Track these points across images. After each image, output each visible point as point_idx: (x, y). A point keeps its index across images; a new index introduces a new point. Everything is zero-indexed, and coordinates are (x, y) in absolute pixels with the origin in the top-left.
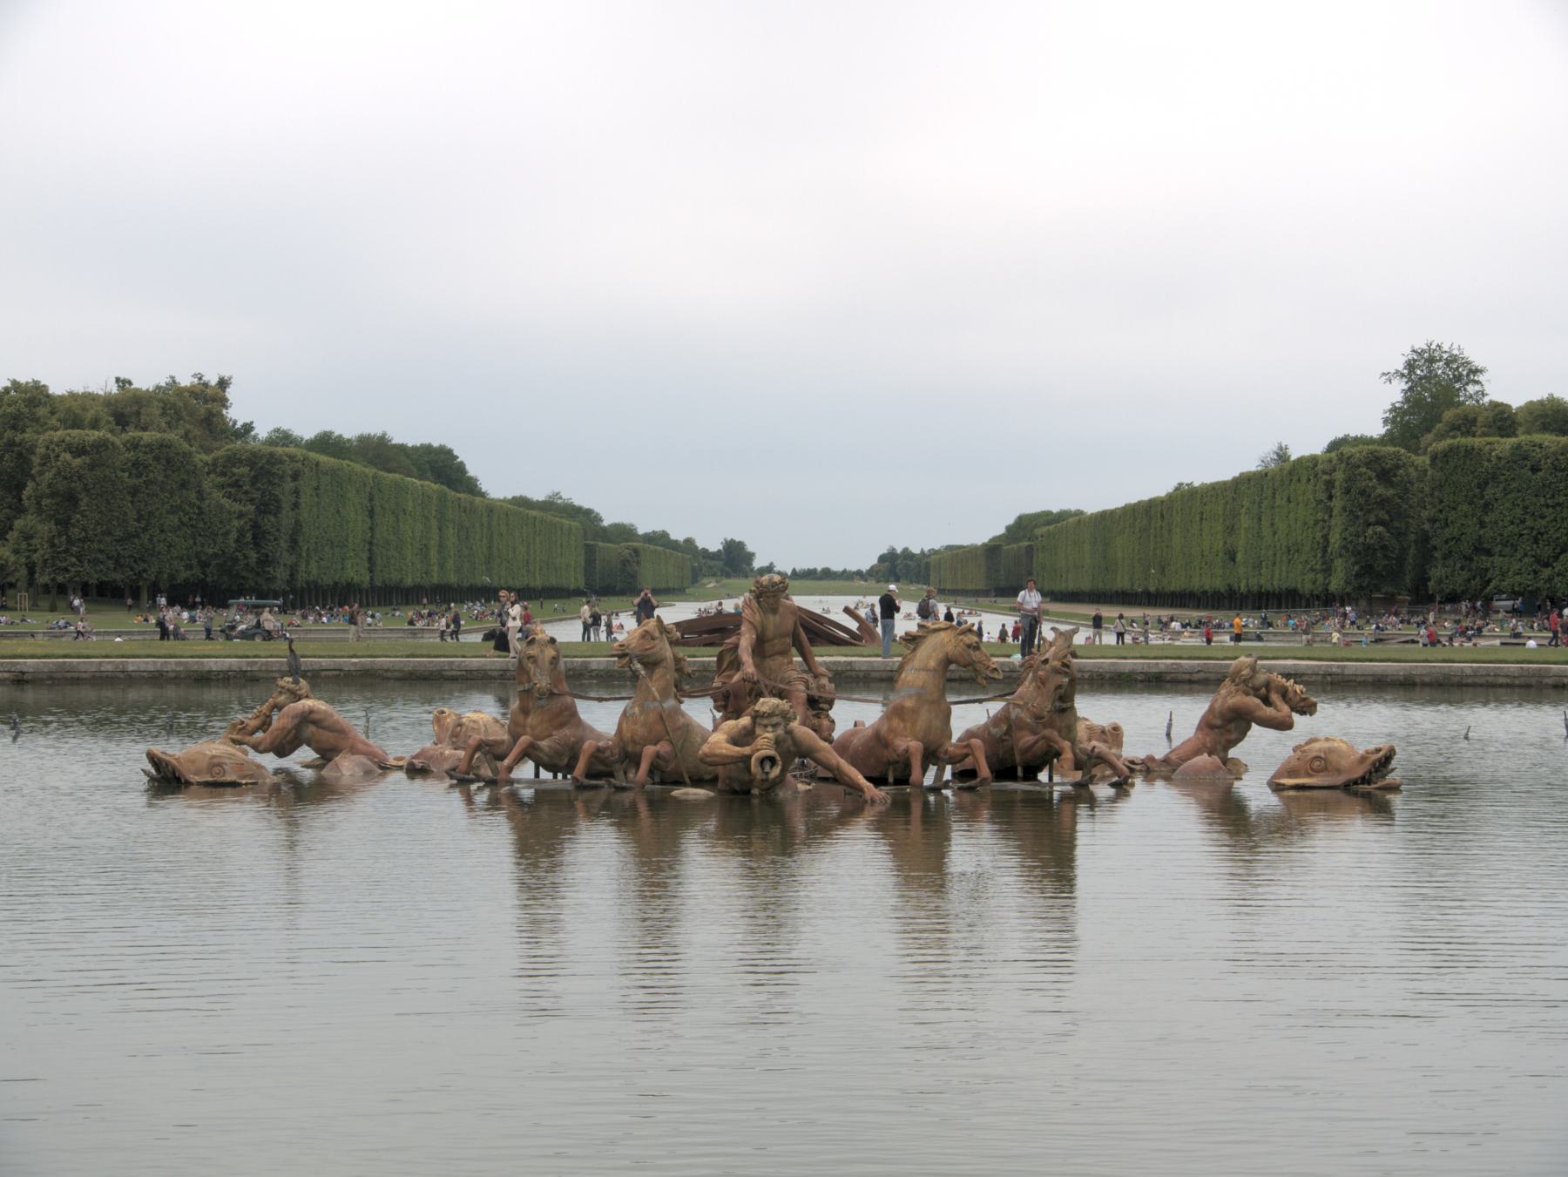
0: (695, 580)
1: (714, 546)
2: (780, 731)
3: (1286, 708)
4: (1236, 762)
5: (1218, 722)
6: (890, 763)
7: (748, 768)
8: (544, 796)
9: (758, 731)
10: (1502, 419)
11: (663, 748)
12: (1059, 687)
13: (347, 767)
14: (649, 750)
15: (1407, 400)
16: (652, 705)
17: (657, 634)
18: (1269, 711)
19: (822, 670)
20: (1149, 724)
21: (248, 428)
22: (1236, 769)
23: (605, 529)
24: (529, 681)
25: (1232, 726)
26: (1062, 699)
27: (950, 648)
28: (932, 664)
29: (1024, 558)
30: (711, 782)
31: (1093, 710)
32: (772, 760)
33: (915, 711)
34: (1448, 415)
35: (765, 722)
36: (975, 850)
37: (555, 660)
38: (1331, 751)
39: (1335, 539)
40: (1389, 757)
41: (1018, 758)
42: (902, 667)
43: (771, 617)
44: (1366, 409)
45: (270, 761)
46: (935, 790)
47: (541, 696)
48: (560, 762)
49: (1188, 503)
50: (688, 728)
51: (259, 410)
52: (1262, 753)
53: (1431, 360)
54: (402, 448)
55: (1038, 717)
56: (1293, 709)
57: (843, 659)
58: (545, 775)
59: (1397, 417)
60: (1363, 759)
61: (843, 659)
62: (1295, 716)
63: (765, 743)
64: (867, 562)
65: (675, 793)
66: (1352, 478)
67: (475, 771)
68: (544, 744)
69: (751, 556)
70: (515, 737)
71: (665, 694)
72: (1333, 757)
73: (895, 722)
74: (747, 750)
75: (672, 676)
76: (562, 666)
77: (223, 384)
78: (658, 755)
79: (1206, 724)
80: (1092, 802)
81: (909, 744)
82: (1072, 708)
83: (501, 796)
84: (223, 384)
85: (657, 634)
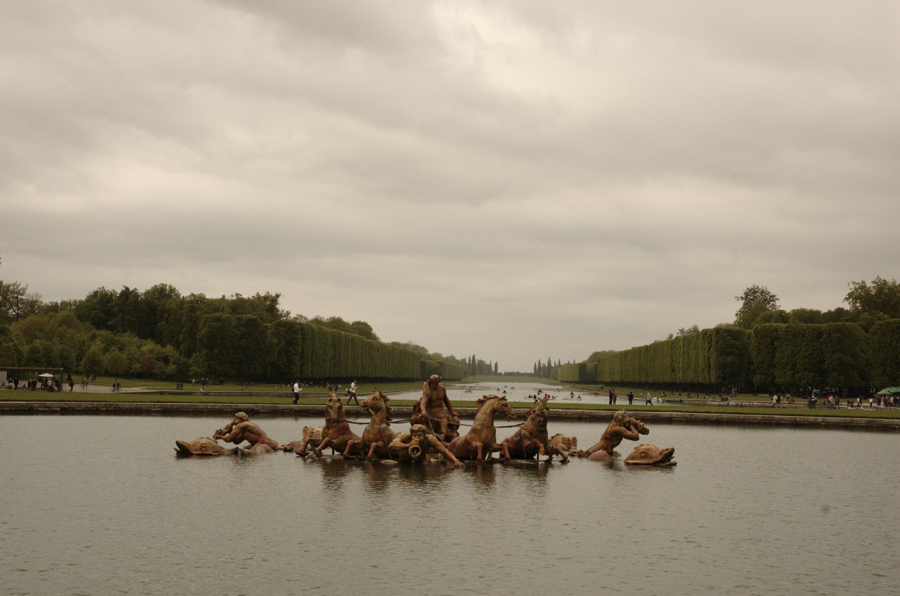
0: (465, 376)
2: (422, 438)
3: (636, 432)
4: (616, 453)
8: (334, 461)
10: (782, 316)
11: (380, 443)
12: (539, 422)
13: (259, 448)
14: (374, 444)
16: (376, 426)
19: (455, 413)
20: (590, 435)
21: (288, 313)
26: (541, 426)
27: (495, 406)
28: (488, 412)
31: (553, 429)
32: (417, 449)
33: (481, 431)
34: (762, 314)
37: (340, 408)
38: (649, 449)
39: (712, 361)
40: (672, 451)
42: (477, 412)
44: (725, 313)
45: (231, 446)
47: (334, 421)
48: (339, 448)
49: (655, 349)
52: (625, 448)
55: (531, 434)
56: (640, 432)
60: (661, 453)
62: (640, 435)
65: (383, 462)
67: (308, 450)
68: (335, 441)
70: (324, 438)
71: (382, 422)
72: (650, 452)
73: (473, 435)
74: (408, 445)
75: (384, 415)
76: (343, 410)
77: (278, 296)
78: (377, 446)
80: (552, 466)
81: (477, 444)
83: (319, 458)
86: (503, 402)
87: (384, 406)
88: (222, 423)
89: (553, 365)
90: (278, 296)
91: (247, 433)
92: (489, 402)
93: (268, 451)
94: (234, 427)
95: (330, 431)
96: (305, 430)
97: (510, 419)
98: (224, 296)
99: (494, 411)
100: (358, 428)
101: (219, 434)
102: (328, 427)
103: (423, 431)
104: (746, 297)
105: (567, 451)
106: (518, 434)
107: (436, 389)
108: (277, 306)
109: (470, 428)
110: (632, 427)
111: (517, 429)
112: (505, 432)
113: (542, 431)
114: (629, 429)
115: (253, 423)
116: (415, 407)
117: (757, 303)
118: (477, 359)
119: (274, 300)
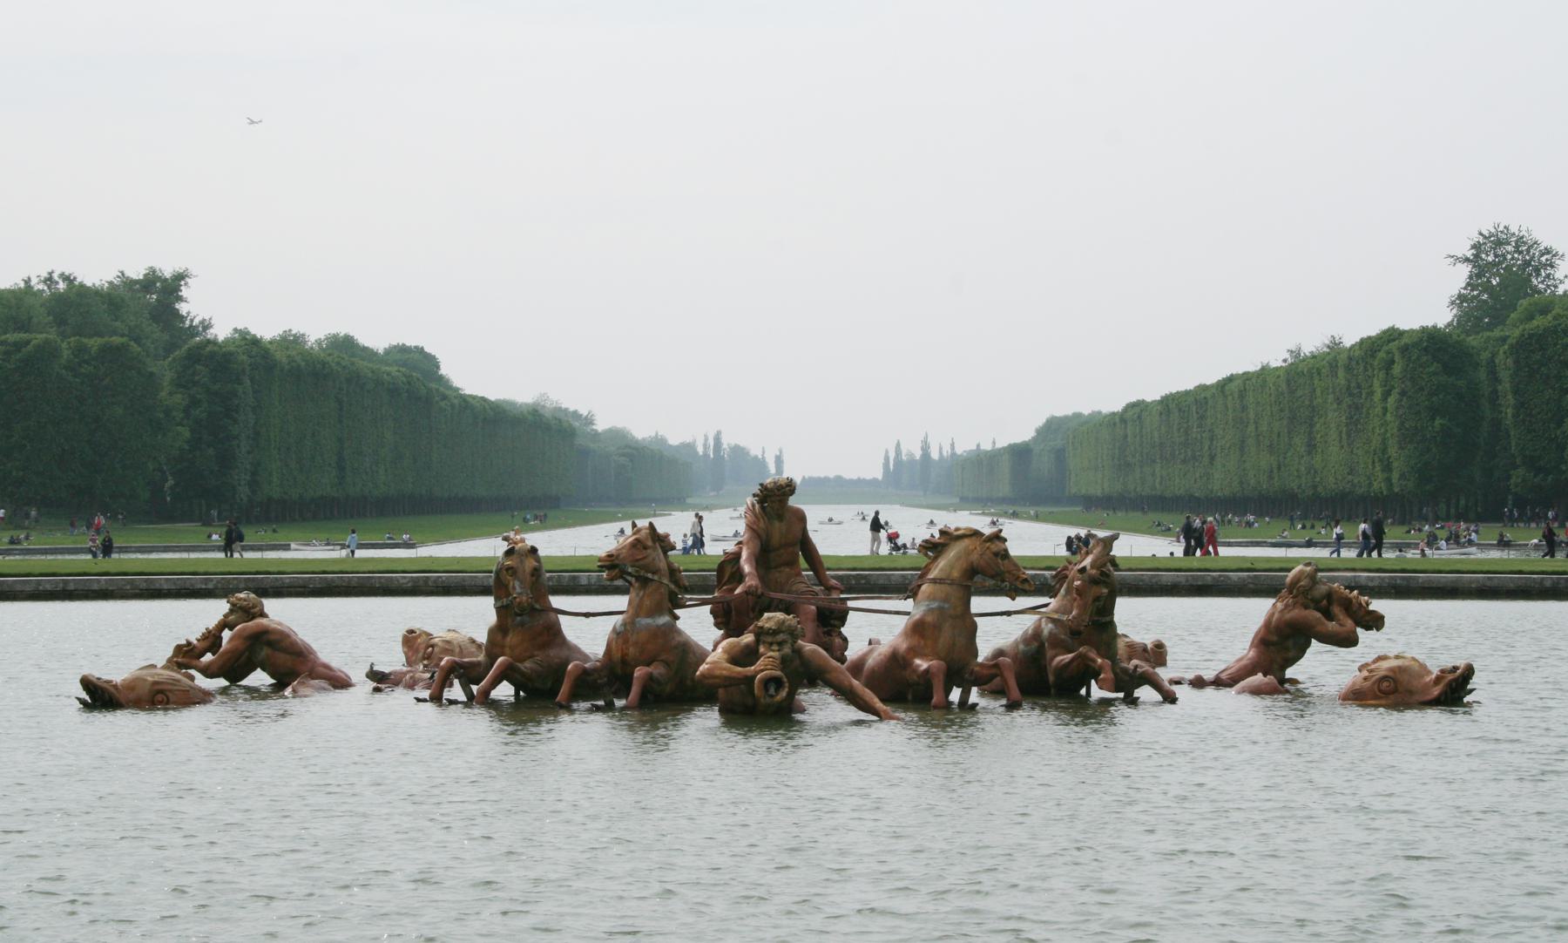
3: (1349, 623)
5: (1275, 638)
9: (762, 649)
11: (657, 670)
12: (1097, 599)
17: (650, 543)
18: (1332, 626)
19: (833, 582)
21: (206, 326)
23: (596, 434)
24: (509, 594)
25: (1290, 643)
27: (975, 557)
28: (956, 574)
29: (1033, 472)
31: (1136, 618)
32: (777, 682)
33: (937, 627)
34: (1524, 303)
35: (770, 639)
40: (1469, 672)
41: (1051, 678)
43: (777, 524)
44: (1428, 300)
51: (220, 308)
52: (1323, 667)
56: (1358, 624)
60: (1438, 680)
62: (1359, 631)
63: (766, 665)
67: (442, 672)
70: (492, 658)
78: (650, 677)
85: (650, 543)
86: (995, 547)
87: (663, 565)
89: (935, 455)
90: (180, 277)
91: (265, 652)
92: (952, 553)
94: (226, 635)
95: (511, 639)
96: (411, 640)
97: (1013, 593)
98: (28, 281)
99: (972, 572)
100: (589, 627)
101: (185, 655)
102: (499, 631)
103: (793, 634)
104: (1477, 256)
105: (1138, 673)
106: (1035, 636)
107: (780, 517)
108: (183, 308)
109: (901, 623)
111: (1028, 621)
112: (1000, 626)
113: (1100, 625)
114: (1329, 616)
115: (281, 612)
116: (721, 568)
118: (727, 441)
119: (160, 294)
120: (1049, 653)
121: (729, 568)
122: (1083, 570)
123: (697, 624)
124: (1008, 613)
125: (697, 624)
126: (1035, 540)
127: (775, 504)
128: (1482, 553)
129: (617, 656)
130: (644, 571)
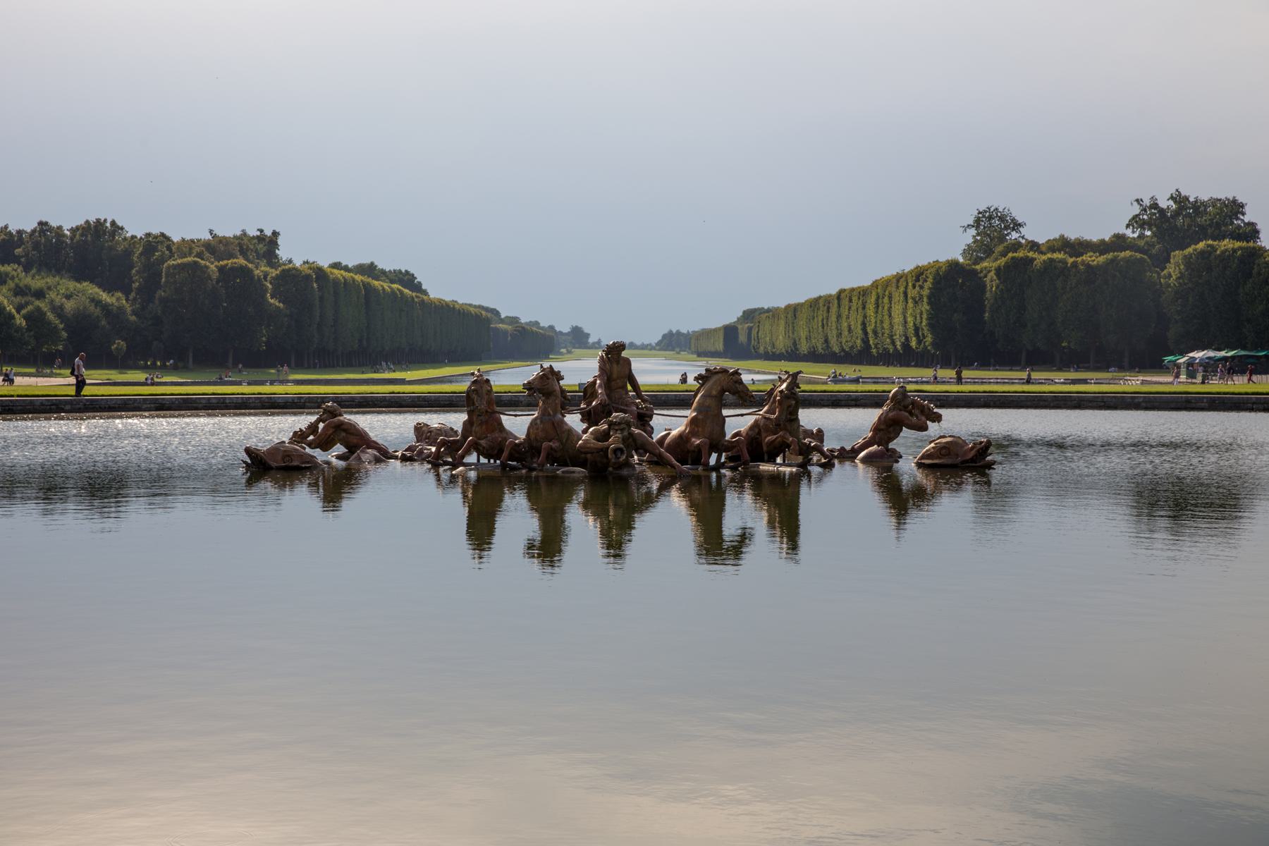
1: (566, 329)
3: (923, 418)
4: (894, 451)
6: (688, 451)
7: (607, 456)
11: (555, 444)
15: (976, 241)
20: (854, 424)
22: (895, 456)
30: (582, 464)
31: (809, 418)
36: (742, 511)
41: (765, 449)
46: (717, 468)
48: (491, 452)
50: (570, 431)
52: (910, 448)
53: (990, 218)
54: (563, 512)
57: (267, 389)
58: (483, 460)
59: (968, 251)
60: (972, 448)
61: (267, 389)
63: (614, 441)
64: (655, 338)
66: (949, 288)
67: (438, 453)
68: (483, 442)
69: (588, 335)
77: (275, 234)
79: (877, 429)
82: (797, 420)
84: (275, 234)
87: (557, 388)
88: (303, 421)
93: (378, 461)
94: (321, 425)
101: (299, 437)
102: (468, 425)
103: (629, 425)
109: (685, 421)
110: (916, 412)
111: (755, 417)
112: (738, 422)
117: (993, 228)
119: (268, 244)
120: (763, 435)
121: (588, 391)
122: (781, 392)
123: (574, 421)
124: (103, 487)
125: (574, 421)
126: (755, 376)
127: (615, 358)
128: (172, 385)
129: (533, 437)
130: (545, 390)
